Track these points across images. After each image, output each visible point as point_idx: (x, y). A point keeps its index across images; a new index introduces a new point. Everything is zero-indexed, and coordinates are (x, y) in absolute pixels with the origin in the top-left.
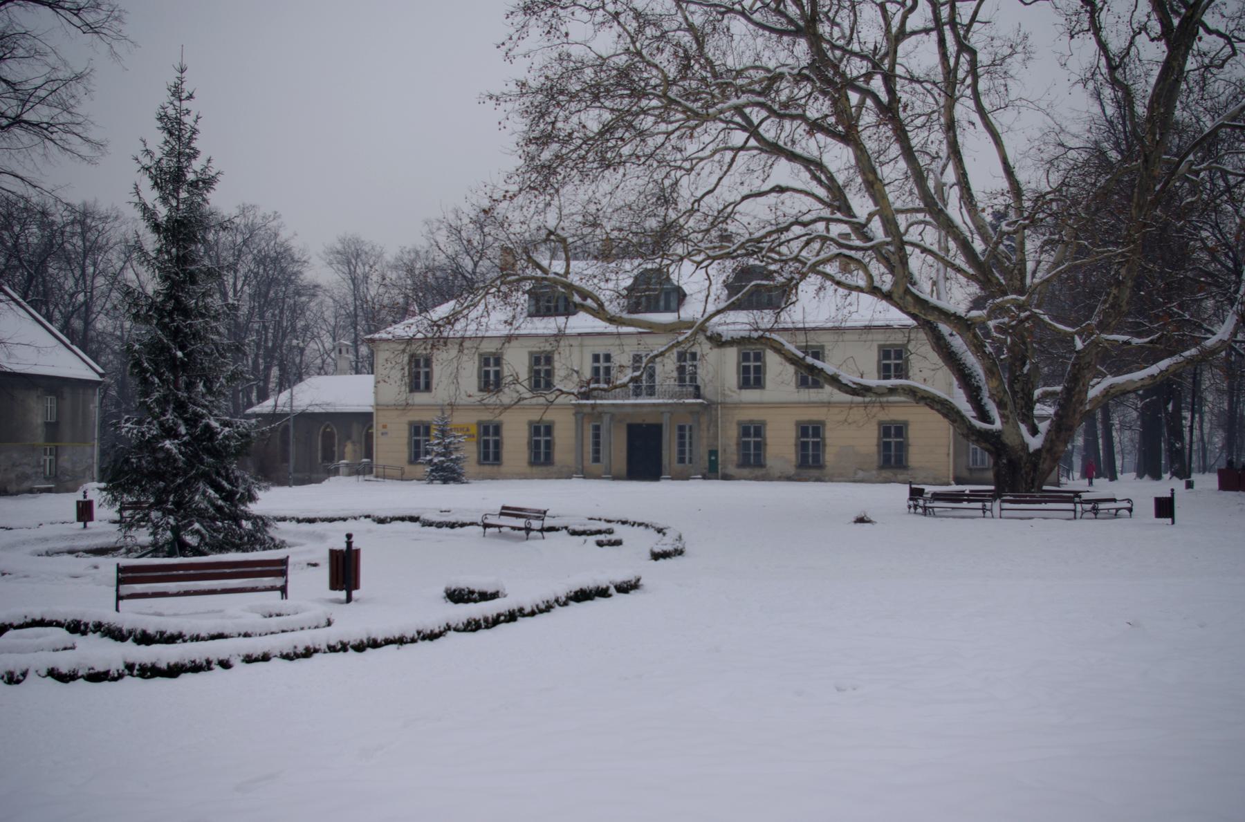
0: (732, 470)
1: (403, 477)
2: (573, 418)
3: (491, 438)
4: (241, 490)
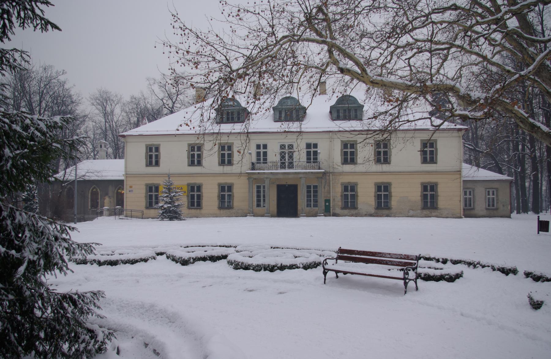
0: (338, 211)
1: (143, 217)
2: (247, 181)
3: (196, 193)
4: (28, 255)
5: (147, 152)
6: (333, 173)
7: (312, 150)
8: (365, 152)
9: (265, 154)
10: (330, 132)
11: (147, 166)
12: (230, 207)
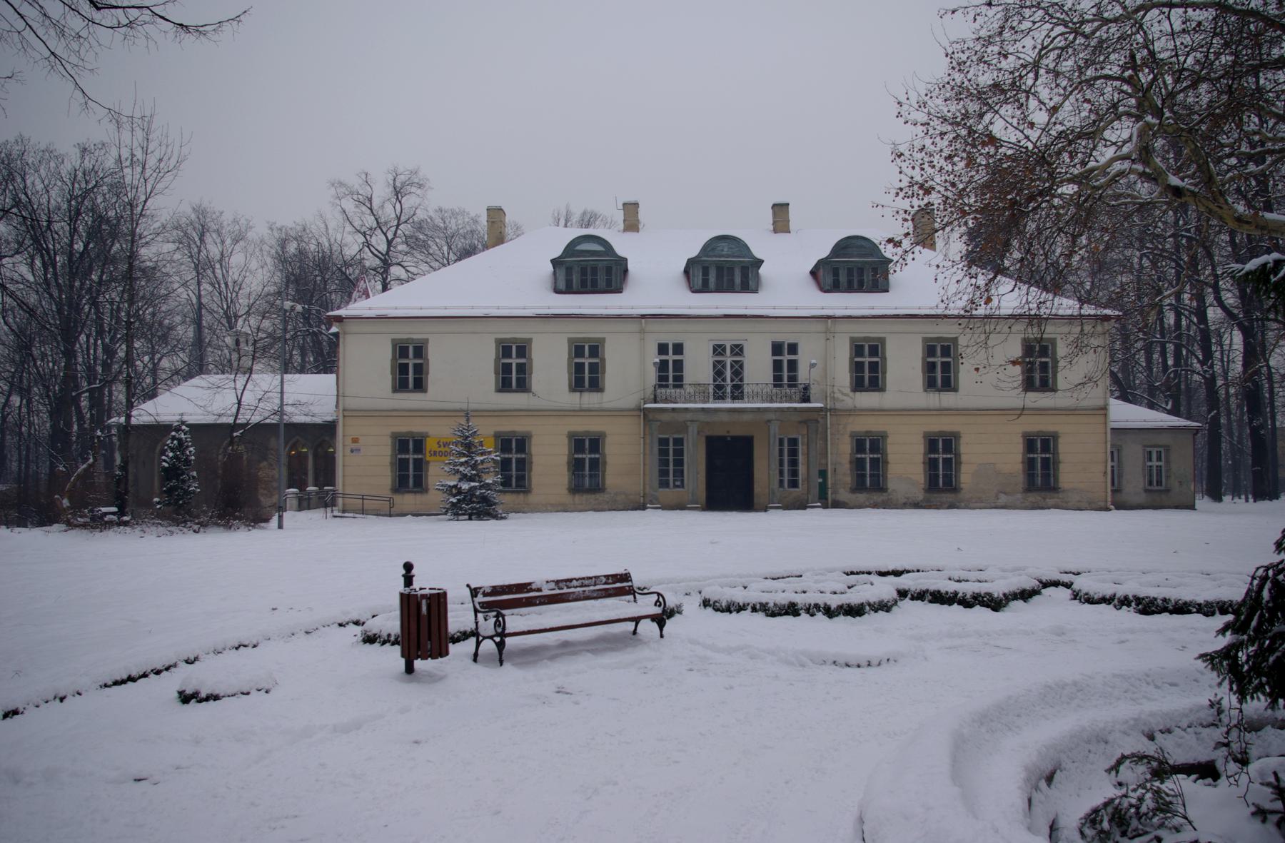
0: (844, 495)
1: (391, 512)
5: (394, 359)
6: (834, 411)
7: (786, 358)
8: (904, 364)
9: (679, 365)
10: (829, 317)
11: (395, 390)
12: (597, 488)
